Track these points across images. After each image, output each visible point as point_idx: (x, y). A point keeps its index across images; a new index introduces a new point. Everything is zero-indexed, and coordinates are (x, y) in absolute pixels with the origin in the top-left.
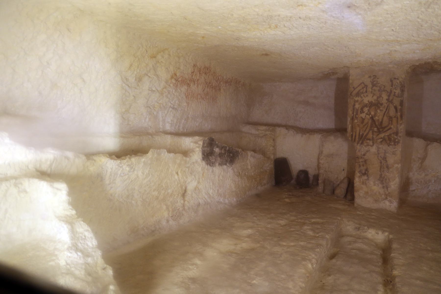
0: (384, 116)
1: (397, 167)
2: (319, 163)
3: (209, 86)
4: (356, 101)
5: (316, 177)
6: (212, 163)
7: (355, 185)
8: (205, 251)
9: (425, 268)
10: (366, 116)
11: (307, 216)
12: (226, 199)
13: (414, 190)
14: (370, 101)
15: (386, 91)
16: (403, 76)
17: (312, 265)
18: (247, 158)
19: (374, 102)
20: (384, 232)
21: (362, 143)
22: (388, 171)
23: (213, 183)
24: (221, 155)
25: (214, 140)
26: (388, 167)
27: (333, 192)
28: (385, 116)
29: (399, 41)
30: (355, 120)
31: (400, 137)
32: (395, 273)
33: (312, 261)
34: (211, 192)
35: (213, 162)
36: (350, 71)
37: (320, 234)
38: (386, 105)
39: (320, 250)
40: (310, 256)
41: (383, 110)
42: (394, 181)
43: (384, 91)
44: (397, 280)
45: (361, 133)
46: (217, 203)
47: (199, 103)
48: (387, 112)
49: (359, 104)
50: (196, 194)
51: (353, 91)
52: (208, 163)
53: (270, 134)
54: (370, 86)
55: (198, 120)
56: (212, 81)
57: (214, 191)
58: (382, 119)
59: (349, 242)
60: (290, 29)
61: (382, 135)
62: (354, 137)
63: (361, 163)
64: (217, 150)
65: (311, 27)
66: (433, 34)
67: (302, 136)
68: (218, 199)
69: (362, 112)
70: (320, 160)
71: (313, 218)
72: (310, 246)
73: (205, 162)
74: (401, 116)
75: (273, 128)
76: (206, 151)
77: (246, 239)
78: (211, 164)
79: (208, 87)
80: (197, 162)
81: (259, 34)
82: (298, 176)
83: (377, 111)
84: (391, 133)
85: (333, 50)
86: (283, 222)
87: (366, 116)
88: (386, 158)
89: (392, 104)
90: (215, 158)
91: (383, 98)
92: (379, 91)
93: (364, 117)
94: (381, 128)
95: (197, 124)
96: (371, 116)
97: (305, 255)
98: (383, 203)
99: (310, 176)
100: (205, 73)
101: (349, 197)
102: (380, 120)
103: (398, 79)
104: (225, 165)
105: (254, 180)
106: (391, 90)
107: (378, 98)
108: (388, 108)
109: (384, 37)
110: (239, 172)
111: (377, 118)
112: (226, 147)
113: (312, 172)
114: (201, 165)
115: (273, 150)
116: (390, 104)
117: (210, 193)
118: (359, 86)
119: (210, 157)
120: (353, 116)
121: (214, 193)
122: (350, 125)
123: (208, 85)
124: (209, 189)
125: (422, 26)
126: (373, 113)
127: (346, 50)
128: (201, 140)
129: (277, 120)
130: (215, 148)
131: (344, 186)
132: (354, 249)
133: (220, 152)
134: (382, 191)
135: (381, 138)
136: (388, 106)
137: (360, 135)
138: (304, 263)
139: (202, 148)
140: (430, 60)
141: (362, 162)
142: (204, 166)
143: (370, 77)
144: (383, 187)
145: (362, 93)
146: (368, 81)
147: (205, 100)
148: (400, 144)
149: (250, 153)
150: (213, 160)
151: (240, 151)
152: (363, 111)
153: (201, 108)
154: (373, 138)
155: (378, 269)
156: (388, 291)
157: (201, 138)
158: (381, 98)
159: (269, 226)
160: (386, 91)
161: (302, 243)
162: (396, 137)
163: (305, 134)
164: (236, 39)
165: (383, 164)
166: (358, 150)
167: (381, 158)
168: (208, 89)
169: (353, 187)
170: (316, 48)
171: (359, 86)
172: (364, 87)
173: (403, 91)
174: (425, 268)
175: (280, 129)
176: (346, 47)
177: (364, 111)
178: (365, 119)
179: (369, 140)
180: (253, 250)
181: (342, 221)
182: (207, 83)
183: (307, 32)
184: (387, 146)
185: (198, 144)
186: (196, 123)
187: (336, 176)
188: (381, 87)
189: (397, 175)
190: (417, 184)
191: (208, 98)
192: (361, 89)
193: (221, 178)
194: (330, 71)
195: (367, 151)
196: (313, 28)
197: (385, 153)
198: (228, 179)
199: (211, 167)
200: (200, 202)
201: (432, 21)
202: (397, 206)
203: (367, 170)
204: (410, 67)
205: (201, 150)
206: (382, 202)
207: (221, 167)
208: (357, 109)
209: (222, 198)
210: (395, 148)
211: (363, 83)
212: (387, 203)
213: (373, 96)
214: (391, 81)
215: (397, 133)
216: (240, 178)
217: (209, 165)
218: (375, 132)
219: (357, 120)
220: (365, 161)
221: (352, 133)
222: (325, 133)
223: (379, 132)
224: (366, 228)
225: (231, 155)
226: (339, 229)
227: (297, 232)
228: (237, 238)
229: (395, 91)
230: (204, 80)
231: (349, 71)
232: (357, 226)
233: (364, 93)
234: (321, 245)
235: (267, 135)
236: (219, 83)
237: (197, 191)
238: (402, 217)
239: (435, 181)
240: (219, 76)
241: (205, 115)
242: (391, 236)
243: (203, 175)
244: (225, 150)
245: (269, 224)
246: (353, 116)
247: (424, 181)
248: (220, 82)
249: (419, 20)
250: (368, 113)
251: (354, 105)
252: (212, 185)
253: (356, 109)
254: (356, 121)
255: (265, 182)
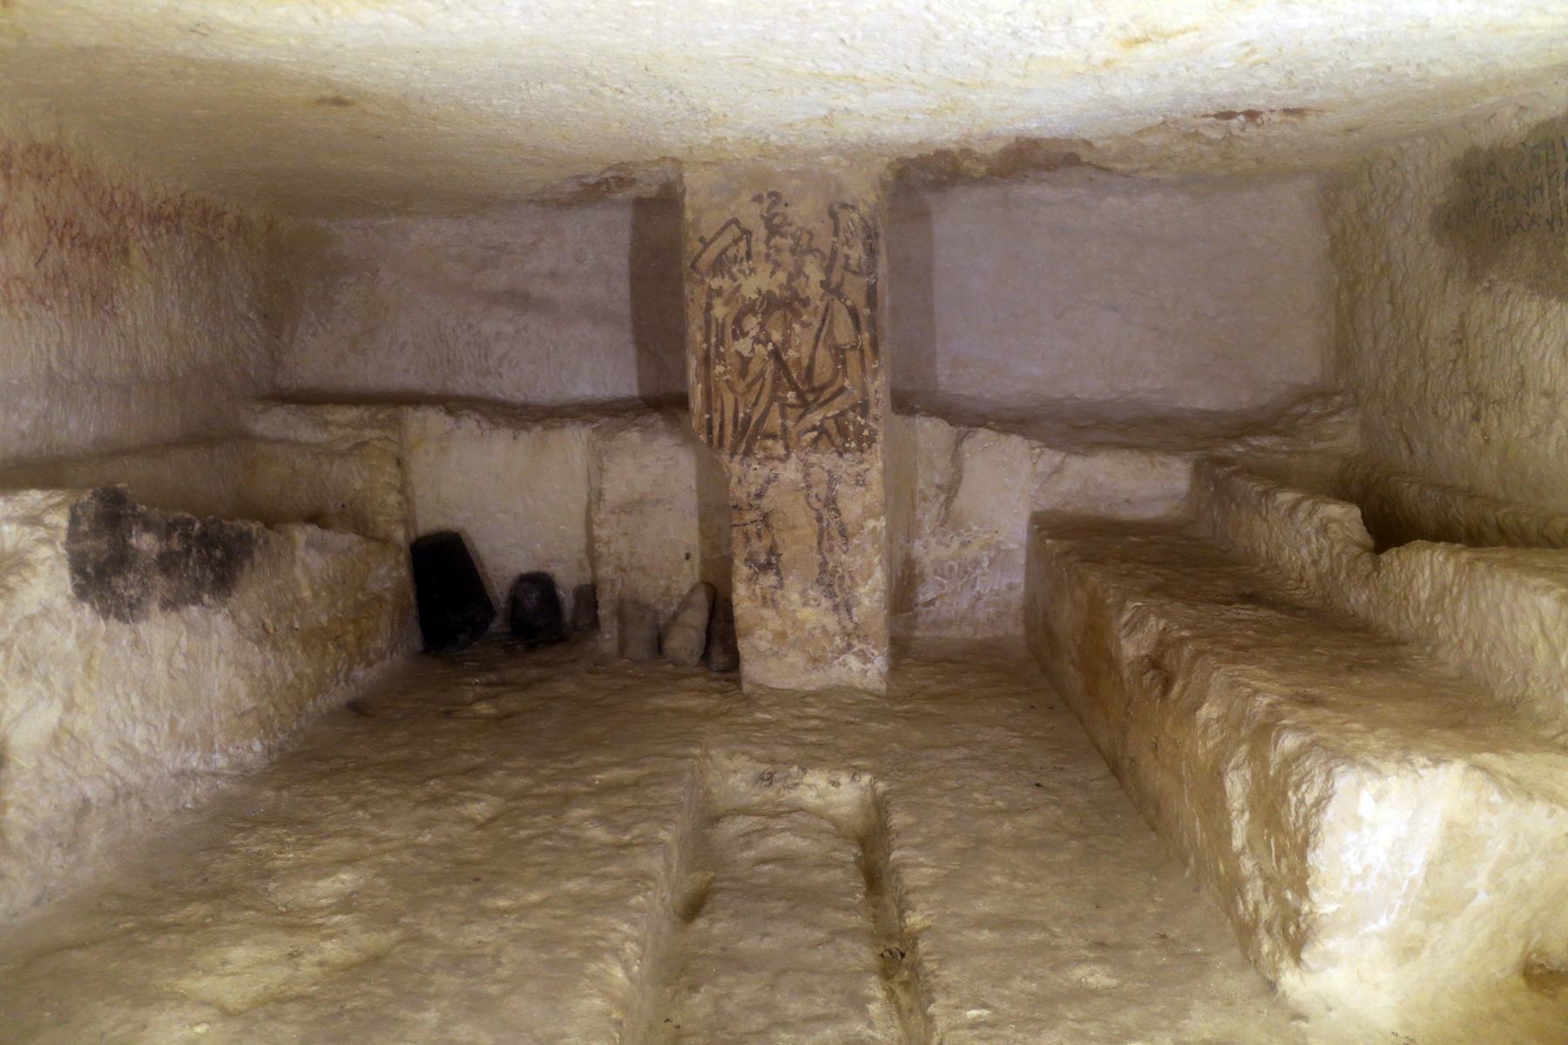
0: (815, 347)
1: (875, 528)
2: (591, 540)
3: (67, 240)
4: (713, 290)
5: (588, 596)
6: (131, 606)
7: (738, 612)
8: (144, 1027)
9: (998, 879)
10: (753, 350)
11: (571, 762)
12: (215, 752)
13: (931, 602)
14: (764, 292)
15: (816, 253)
16: (871, 198)
17: (626, 967)
18: (293, 554)
19: (777, 291)
20: (855, 772)
21: (748, 452)
22: (845, 548)
23: (145, 696)
24: (166, 563)
25: (128, 498)
26: (843, 533)
27: (658, 645)
28: (820, 344)
29: (863, 80)
30: (715, 364)
31: (876, 419)
32: (914, 920)
33: (623, 950)
34: (138, 735)
35: (133, 601)
36: (686, 175)
37: (636, 832)
38: (822, 305)
39: (644, 897)
40: (613, 936)
41: (811, 324)
42: (870, 582)
43: (811, 250)
44: (923, 946)
45: (741, 415)
46: (172, 781)
47: (24, 323)
48: (825, 330)
49: (727, 303)
50: (65, 762)
51: (699, 255)
52: (110, 606)
53: (379, 439)
54: (761, 232)
55: (24, 402)
56: (81, 214)
57: (152, 728)
58: (812, 358)
59: (743, 836)
60: (447, 8)
61: (815, 418)
62: (716, 431)
63: (752, 528)
64: (145, 543)
65: (540, 7)
66: (969, 66)
67: (515, 438)
68: (178, 760)
69: (739, 333)
70: (595, 526)
71: (599, 767)
72: (604, 888)
73: (93, 606)
74: (875, 345)
75: (390, 411)
76: (92, 555)
77: (338, 918)
78: (122, 609)
79: (61, 241)
80: (46, 612)
81: (303, 20)
82: (515, 600)
83: (792, 329)
84: (847, 407)
85: (621, 97)
86: (479, 809)
87: (753, 350)
88: (834, 502)
89: (839, 299)
90: (142, 579)
91: (808, 277)
92: (793, 251)
93: (746, 353)
94: (810, 393)
95: (25, 425)
96: (770, 347)
97: (594, 932)
98: (840, 665)
99: (560, 593)
100: (40, 177)
101: (719, 659)
102: (805, 363)
103: (853, 208)
104: (194, 604)
105: (331, 647)
106: (832, 249)
107: (791, 278)
108: (826, 317)
109: (813, 61)
110: (264, 625)
111: (792, 353)
112: (190, 523)
113: (567, 579)
114: (74, 623)
115: (400, 504)
116: (833, 300)
117: (137, 744)
118: (720, 233)
119: (118, 582)
120: (708, 350)
121: (154, 740)
122: (698, 383)
123: (63, 233)
124: (128, 722)
125: (936, 37)
126: (777, 336)
127: (671, 101)
128: (58, 505)
129: (401, 373)
130: (134, 533)
131: (697, 618)
132: (765, 861)
133: (161, 547)
134: (831, 622)
135: (814, 428)
136: (827, 310)
137: (740, 420)
138: (593, 967)
139: (66, 545)
140: (952, 146)
141: (752, 522)
142: (88, 627)
143: (758, 199)
144: (836, 608)
145: (735, 260)
146: (752, 216)
147: (51, 308)
148: (878, 447)
149: (302, 534)
150: (132, 592)
151: (258, 530)
152: (742, 329)
153: (37, 346)
154: (785, 429)
155: (855, 920)
156: (899, 991)
157: (58, 497)
158: (803, 280)
159: (427, 838)
160: (818, 250)
161: (573, 886)
162: (863, 422)
163: (527, 429)
164: (193, 31)
165: (828, 525)
166: (734, 480)
167: (819, 500)
168: (65, 254)
169: (729, 619)
170: (553, 86)
171: (720, 233)
172: (740, 239)
173: (872, 251)
174: (998, 879)
175: (419, 414)
176: (670, 89)
177: (746, 330)
178: (751, 359)
179: (774, 436)
180: (374, 960)
181: (708, 761)
182: (56, 222)
183: (522, 27)
184: (836, 454)
185: (46, 526)
186: (16, 417)
187: (662, 582)
188: (799, 239)
189: (876, 560)
190: (939, 578)
191: (69, 294)
192: (730, 246)
193: (183, 666)
194: (609, 174)
195: (769, 481)
196: (544, 14)
197: (832, 479)
198: (213, 664)
199: (127, 622)
200: (90, 794)
201: (969, 26)
202: (886, 669)
203: (772, 551)
204: (890, 166)
205: (65, 552)
206: (836, 662)
207: (174, 616)
208: (720, 321)
209: (198, 754)
210: (861, 462)
211: (736, 222)
212: (854, 662)
213: (773, 273)
214: (833, 215)
215: (863, 408)
216: (268, 648)
217: (112, 616)
218: (792, 406)
219: (725, 366)
220: (765, 518)
221: (707, 416)
222: (606, 419)
223: (805, 406)
224: (795, 769)
225: (218, 554)
226: (701, 791)
227: (548, 843)
228: (294, 922)
229: (846, 250)
230: (37, 210)
231: (681, 177)
232: (763, 768)
233: (742, 259)
234: (646, 876)
235: (365, 443)
236: (116, 222)
237: (66, 749)
238: (906, 707)
239: (992, 562)
240: (113, 188)
241: (62, 377)
242: (881, 786)
243: (88, 666)
244: (186, 536)
245: (427, 831)
246: (708, 350)
247: (960, 564)
248: (122, 219)
249: (931, 18)
250: (762, 337)
251: (709, 307)
252: (142, 704)
253: (717, 325)
254: (719, 369)
255: (380, 643)
